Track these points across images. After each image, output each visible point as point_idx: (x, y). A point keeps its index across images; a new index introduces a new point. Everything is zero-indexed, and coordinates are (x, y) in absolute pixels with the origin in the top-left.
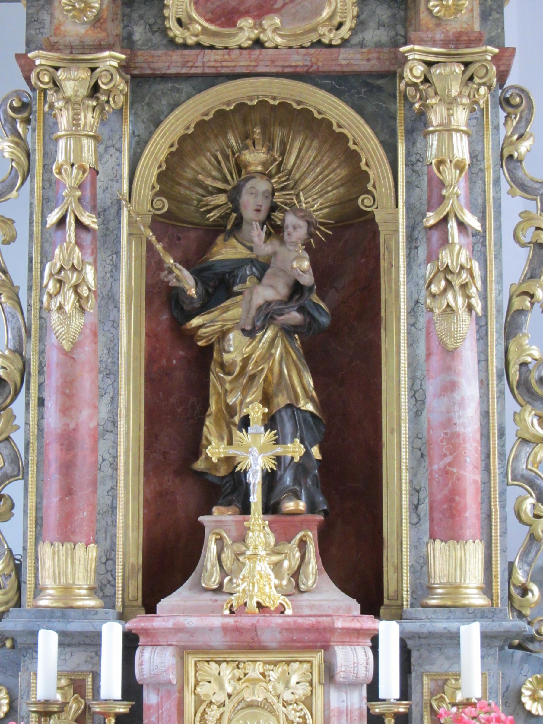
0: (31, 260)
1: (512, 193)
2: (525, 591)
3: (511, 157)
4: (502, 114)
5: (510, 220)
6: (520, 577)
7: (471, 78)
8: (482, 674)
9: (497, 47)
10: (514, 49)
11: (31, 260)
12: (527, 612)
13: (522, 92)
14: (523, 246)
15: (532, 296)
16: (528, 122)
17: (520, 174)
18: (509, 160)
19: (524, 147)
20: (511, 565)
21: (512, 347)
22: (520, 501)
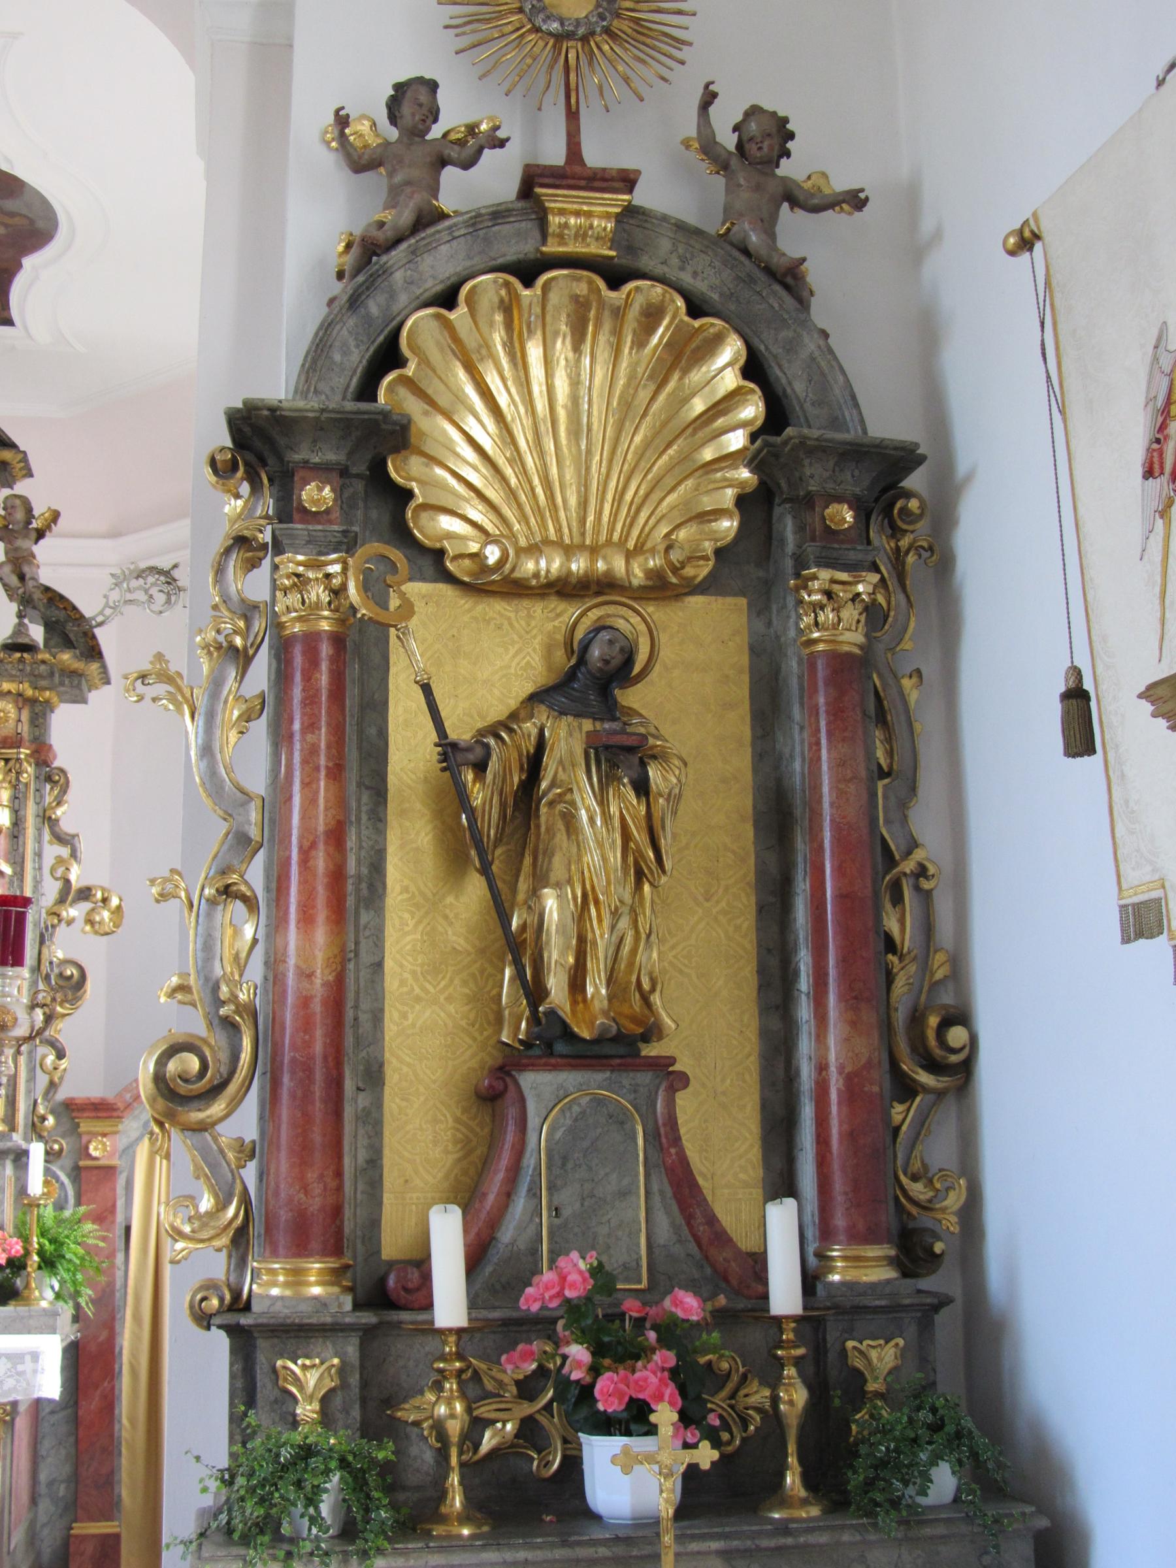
0: (1048, 377)
1: (50, 843)
2: (43, 1119)
3: (50, 818)
4: (48, 787)
5: (48, 861)
6: (41, 1110)
7: (10, 770)
8: (74, 608)
9: (461, 818)
10: (1126, 940)
11: (1048, 377)
12: (45, 1134)
13: (62, 771)
14: (57, 879)
15: (59, 916)
16: (65, 792)
17: (57, 829)
18: (47, 819)
19: (59, 812)
20: (35, 1102)
21: (45, 951)
22: (44, 1057)
